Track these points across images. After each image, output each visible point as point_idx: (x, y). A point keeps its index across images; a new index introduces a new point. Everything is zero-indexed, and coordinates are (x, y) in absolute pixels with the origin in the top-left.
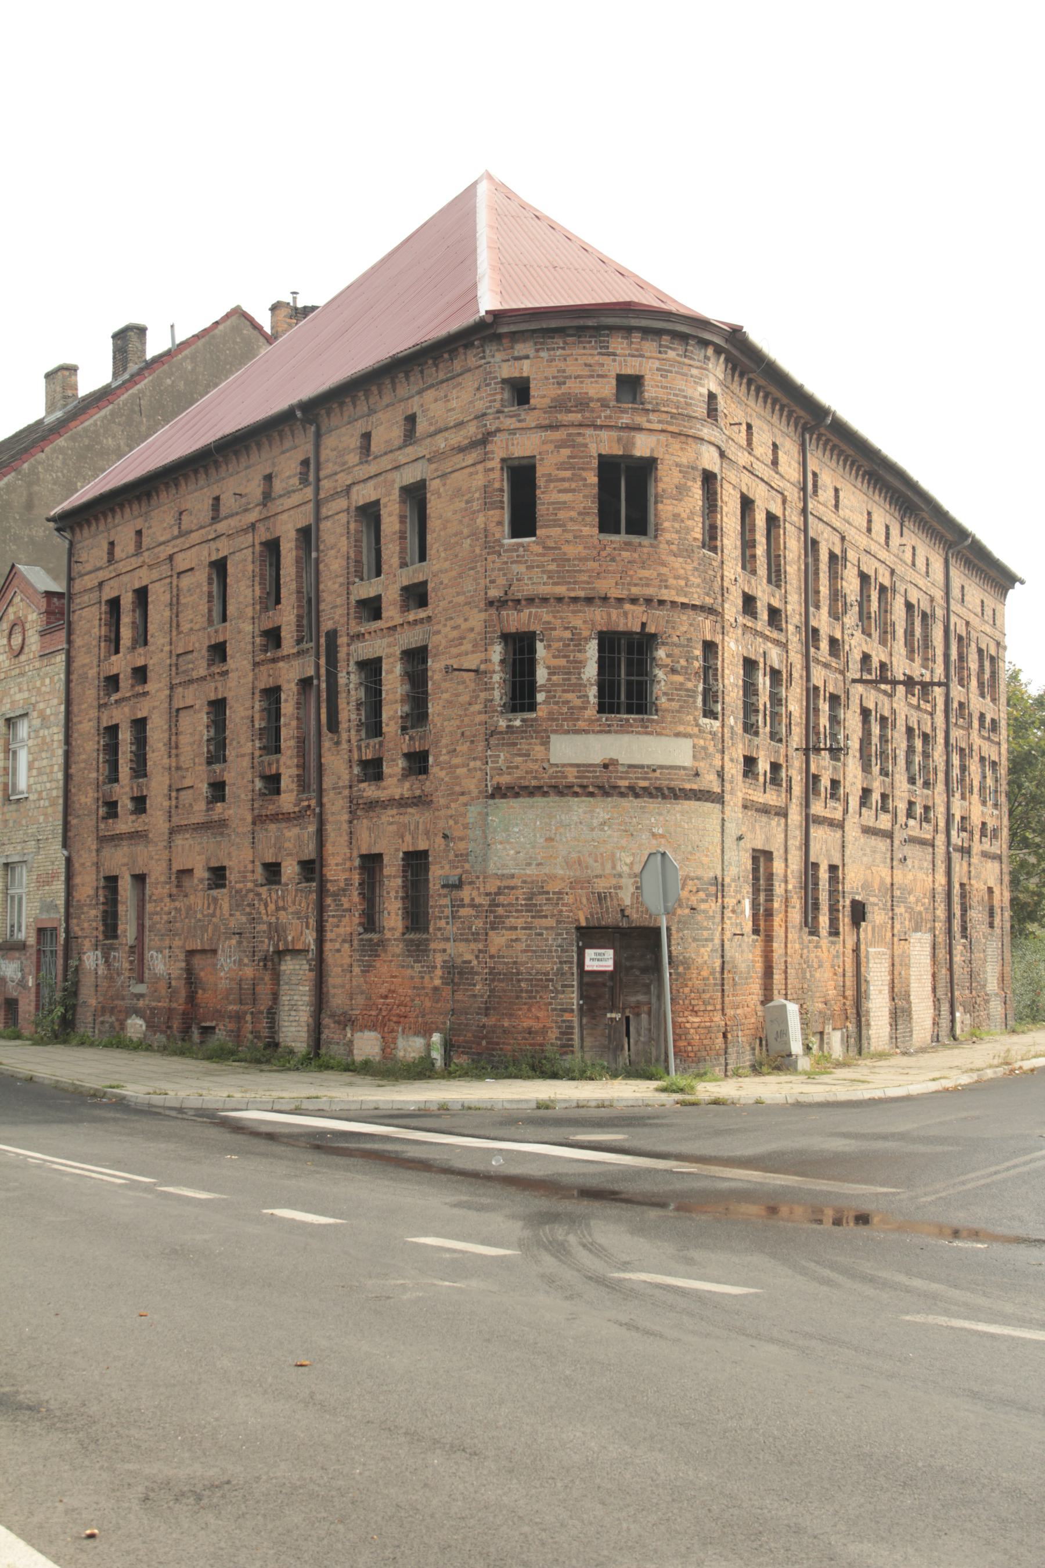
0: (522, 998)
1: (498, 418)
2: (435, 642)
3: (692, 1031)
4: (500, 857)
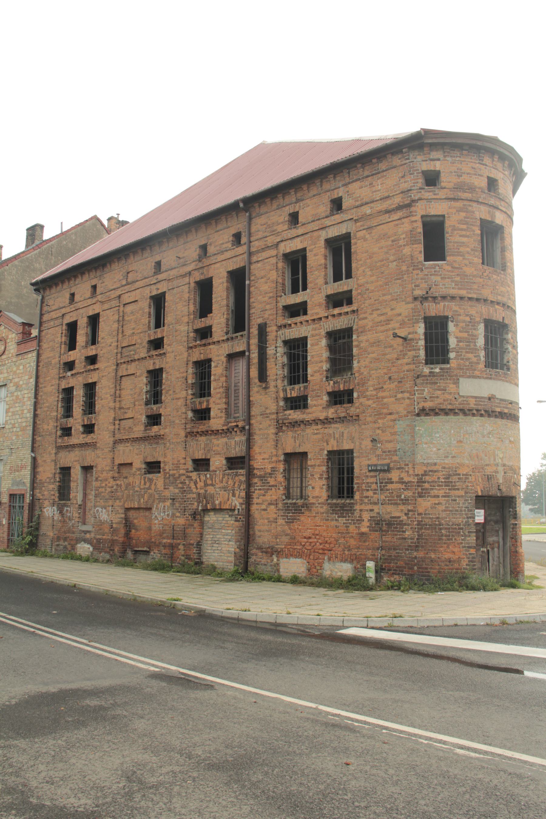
0: (443, 540)
1: (421, 192)
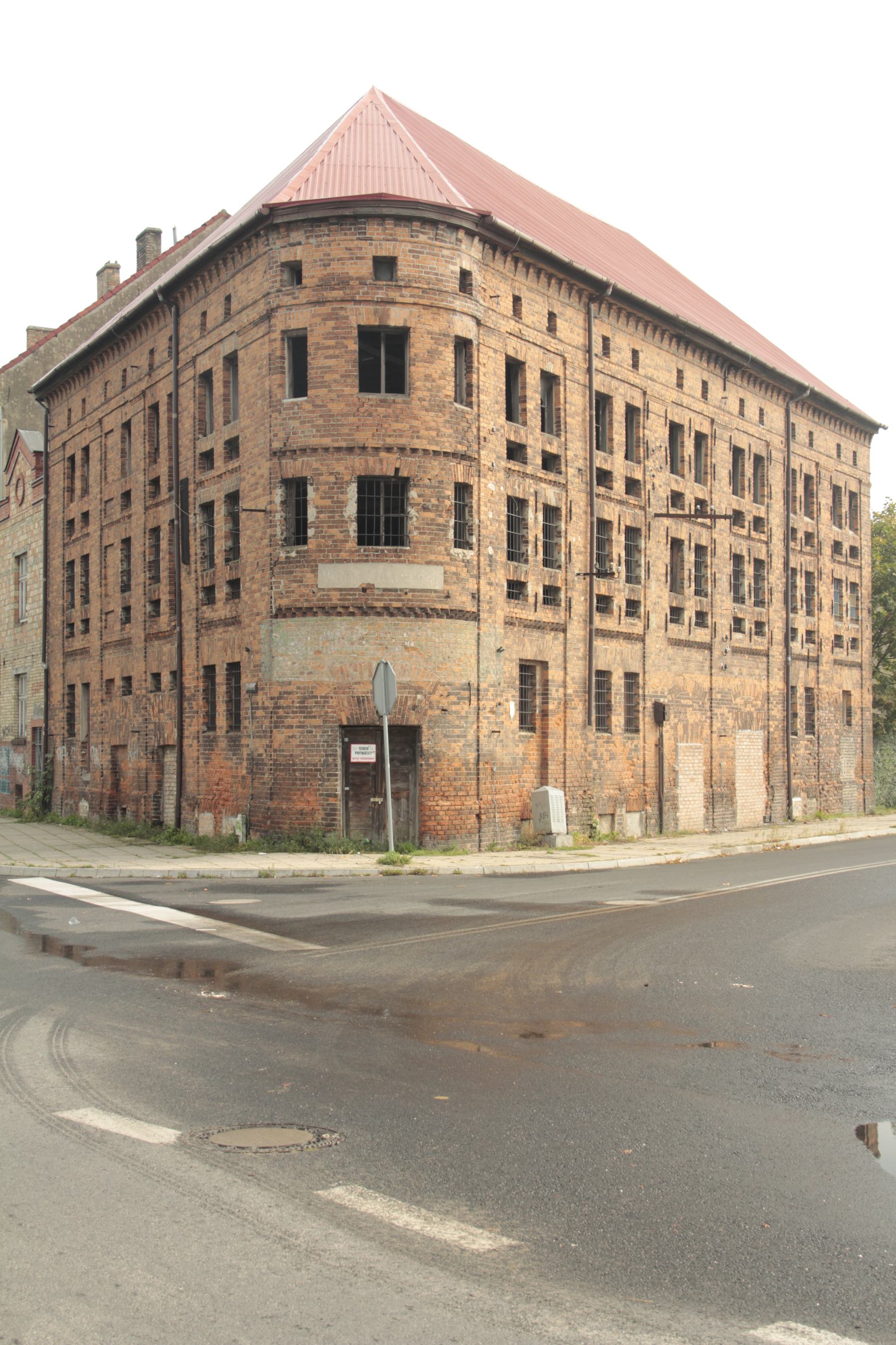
2: (244, 487)
3: (441, 813)
4: (281, 667)
